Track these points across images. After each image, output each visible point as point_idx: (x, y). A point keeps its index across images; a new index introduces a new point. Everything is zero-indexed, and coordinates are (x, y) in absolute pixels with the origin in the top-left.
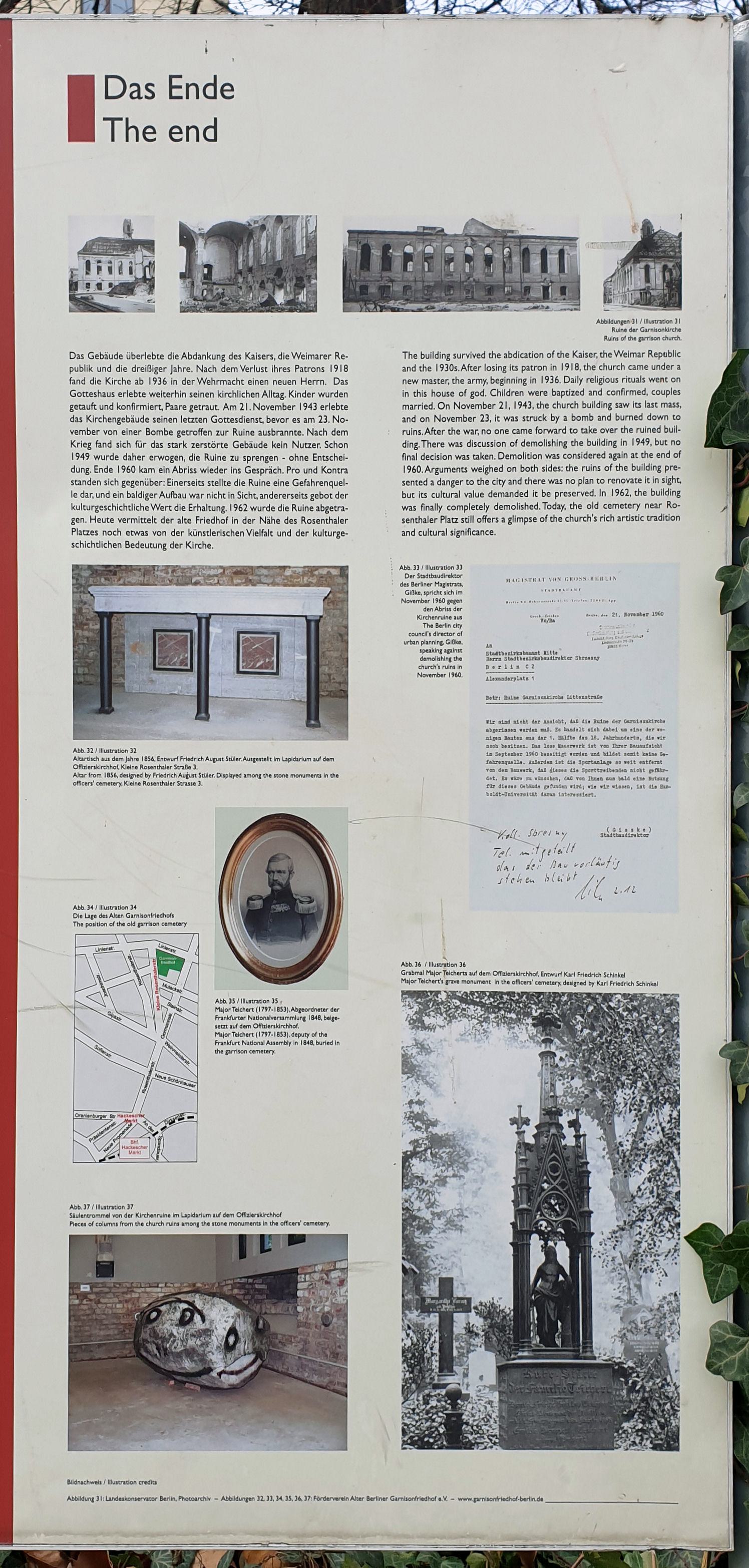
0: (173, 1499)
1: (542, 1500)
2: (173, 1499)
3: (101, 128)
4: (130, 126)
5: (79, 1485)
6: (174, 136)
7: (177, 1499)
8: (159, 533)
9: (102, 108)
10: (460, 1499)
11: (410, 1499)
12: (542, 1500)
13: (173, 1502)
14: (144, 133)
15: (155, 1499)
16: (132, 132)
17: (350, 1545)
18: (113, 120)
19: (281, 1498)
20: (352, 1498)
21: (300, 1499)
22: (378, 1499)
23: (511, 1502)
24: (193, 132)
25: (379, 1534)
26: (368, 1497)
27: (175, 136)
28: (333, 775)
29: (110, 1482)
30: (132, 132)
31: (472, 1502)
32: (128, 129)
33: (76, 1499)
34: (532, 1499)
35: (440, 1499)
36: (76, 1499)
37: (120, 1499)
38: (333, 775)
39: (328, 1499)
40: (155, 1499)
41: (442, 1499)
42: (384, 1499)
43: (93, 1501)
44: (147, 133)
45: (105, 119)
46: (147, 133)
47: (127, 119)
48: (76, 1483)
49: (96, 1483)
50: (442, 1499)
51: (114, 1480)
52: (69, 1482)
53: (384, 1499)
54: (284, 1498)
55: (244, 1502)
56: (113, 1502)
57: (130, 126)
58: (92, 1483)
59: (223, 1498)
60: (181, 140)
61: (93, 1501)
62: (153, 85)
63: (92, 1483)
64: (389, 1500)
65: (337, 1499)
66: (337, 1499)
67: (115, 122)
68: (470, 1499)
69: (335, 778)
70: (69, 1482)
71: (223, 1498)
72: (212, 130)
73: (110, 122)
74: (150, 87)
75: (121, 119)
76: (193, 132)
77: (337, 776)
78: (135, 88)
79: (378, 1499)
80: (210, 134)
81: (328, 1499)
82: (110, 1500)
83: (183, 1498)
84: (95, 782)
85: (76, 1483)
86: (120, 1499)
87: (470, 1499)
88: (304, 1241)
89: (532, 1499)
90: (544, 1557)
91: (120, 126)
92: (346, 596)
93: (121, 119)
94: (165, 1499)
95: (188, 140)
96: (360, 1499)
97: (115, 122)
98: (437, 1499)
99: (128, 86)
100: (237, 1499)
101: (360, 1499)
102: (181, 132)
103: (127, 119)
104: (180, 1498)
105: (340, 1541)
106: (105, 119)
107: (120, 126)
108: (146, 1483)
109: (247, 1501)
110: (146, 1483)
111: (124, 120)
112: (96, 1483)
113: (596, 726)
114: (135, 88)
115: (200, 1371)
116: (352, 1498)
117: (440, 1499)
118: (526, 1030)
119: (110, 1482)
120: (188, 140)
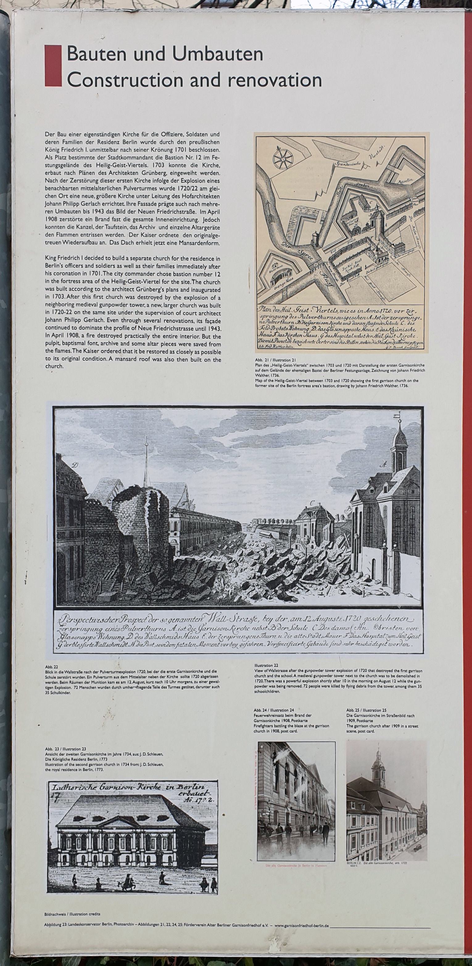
1: (328, 926)
6: (240, 83)
7: (113, 924)
9: (67, 66)
10: (276, 926)
12: (328, 926)
15: (99, 924)
17: (107, 953)
19: (175, 925)
20: (208, 925)
22: (224, 925)
23: (308, 928)
24: (251, 81)
25: (166, 948)
27: (240, 83)
28: (414, 381)
29: (71, 914)
34: (322, 926)
35: (263, 926)
37: (77, 925)
38: (414, 381)
40: (99, 924)
41: (265, 925)
42: (228, 926)
43: (60, 926)
48: (50, 915)
49: (62, 915)
50: (265, 925)
51: (74, 913)
52: (46, 914)
53: (228, 926)
54: (177, 925)
56: (73, 926)
58: (60, 915)
59: (139, 924)
60: (244, 85)
61: (60, 926)
63: (60, 915)
64: (231, 926)
65: (199, 925)
68: (282, 926)
69: (416, 383)
70: (46, 914)
71: (139, 924)
76: (251, 81)
77: (417, 381)
78: (83, 54)
79: (224, 925)
81: (193, 925)
82: (71, 925)
83: (117, 924)
85: (50, 915)
86: (77, 925)
87: (282, 926)
88: (75, 818)
89: (322, 926)
90: (59, 959)
95: (248, 86)
96: (213, 925)
98: (262, 925)
99: (215, 53)
100: (148, 925)
101: (213, 925)
102: (244, 81)
104: (115, 923)
105: (139, 951)
108: (93, 914)
110: (93, 914)
112: (62, 915)
114: (219, 54)
116: (208, 925)
117: (263, 926)
119: (71, 914)
120: (248, 86)
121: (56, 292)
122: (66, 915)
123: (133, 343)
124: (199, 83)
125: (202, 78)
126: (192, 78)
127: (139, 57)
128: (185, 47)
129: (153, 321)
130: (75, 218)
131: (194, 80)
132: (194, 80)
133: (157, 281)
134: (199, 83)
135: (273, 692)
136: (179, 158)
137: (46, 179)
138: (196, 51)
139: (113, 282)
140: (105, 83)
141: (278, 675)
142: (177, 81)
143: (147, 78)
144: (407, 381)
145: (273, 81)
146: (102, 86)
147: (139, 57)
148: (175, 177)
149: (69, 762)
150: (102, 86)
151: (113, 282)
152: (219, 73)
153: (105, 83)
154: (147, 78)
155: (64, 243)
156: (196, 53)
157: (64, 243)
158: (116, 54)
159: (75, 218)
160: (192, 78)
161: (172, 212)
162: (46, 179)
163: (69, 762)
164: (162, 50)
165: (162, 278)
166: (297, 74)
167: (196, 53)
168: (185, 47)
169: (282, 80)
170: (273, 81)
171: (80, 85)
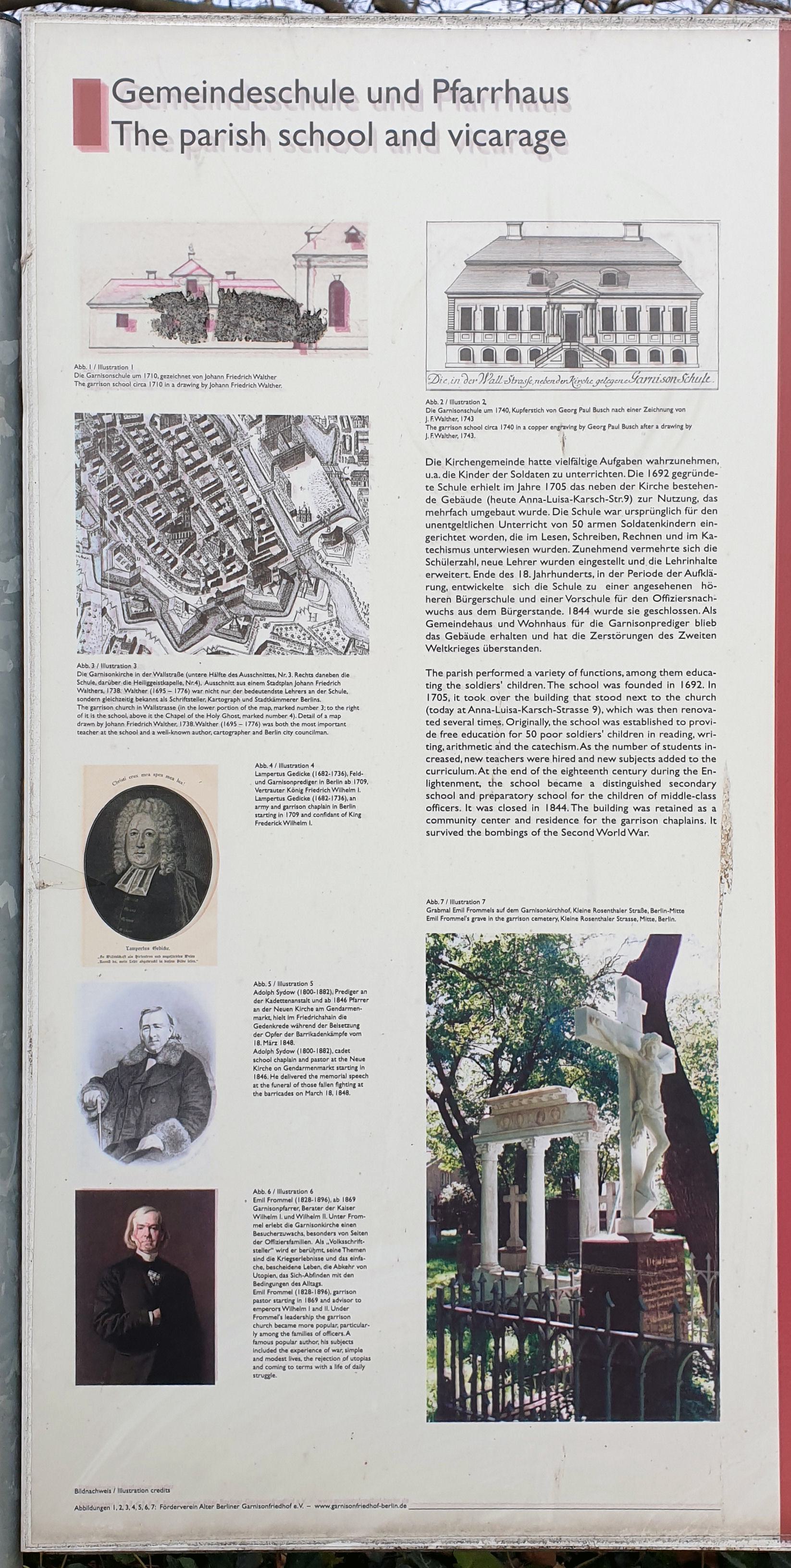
4: (256, 129)
5: (87, 1494)
9: (114, 110)
11: (263, 1507)
12: (405, 1506)
14: (155, 136)
16: (142, 135)
18: (122, 124)
23: (371, 1509)
29: (120, 1491)
30: (142, 135)
31: (330, 1509)
32: (137, 132)
35: (295, 1507)
44: (158, 138)
46: (158, 138)
47: (137, 123)
49: (105, 1491)
55: (99, 1511)
57: (256, 129)
62: (566, 89)
66: (185, 1507)
67: (125, 125)
68: (328, 1507)
73: (119, 125)
74: (563, 92)
75: (130, 123)
78: (529, 92)
80: (428, 138)
84: (606, 733)
87: (328, 1507)
93: (130, 123)
97: (125, 125)
103: (137, 123)
108: (158, 1491)
109: (101, 1511)
110: (158, 1491)
112: (105, 1491)
114: (529, 92)
115: (473, 1367)
119: (120, 1491)
121: (463, 431)
124: (212, 141)
125: (405, 133)
126: (388, 132)
127: (375, 97)
131: (392, 135)
132: (392, 135)
134: (212, 141)
135: (293, 823)
138: (170, 88)
140: (236, 138)
141: (566, 776)
142: (367, 138)
143: (484, 132)
144: (469, 513)
145: (456, 137)
146: (231, 144)
147: (375, 97)
150: (231, 144)
152: (433, 124)
153: (236, 138)
154: (484, 132)
156: (169, 91)
158: (155, 91)
160: (388, 132)
164: (239, 86)
166: (468, 125)
167: (169, 91)
169: (525, 135)
170: (456, 137)
171: (485, 144)
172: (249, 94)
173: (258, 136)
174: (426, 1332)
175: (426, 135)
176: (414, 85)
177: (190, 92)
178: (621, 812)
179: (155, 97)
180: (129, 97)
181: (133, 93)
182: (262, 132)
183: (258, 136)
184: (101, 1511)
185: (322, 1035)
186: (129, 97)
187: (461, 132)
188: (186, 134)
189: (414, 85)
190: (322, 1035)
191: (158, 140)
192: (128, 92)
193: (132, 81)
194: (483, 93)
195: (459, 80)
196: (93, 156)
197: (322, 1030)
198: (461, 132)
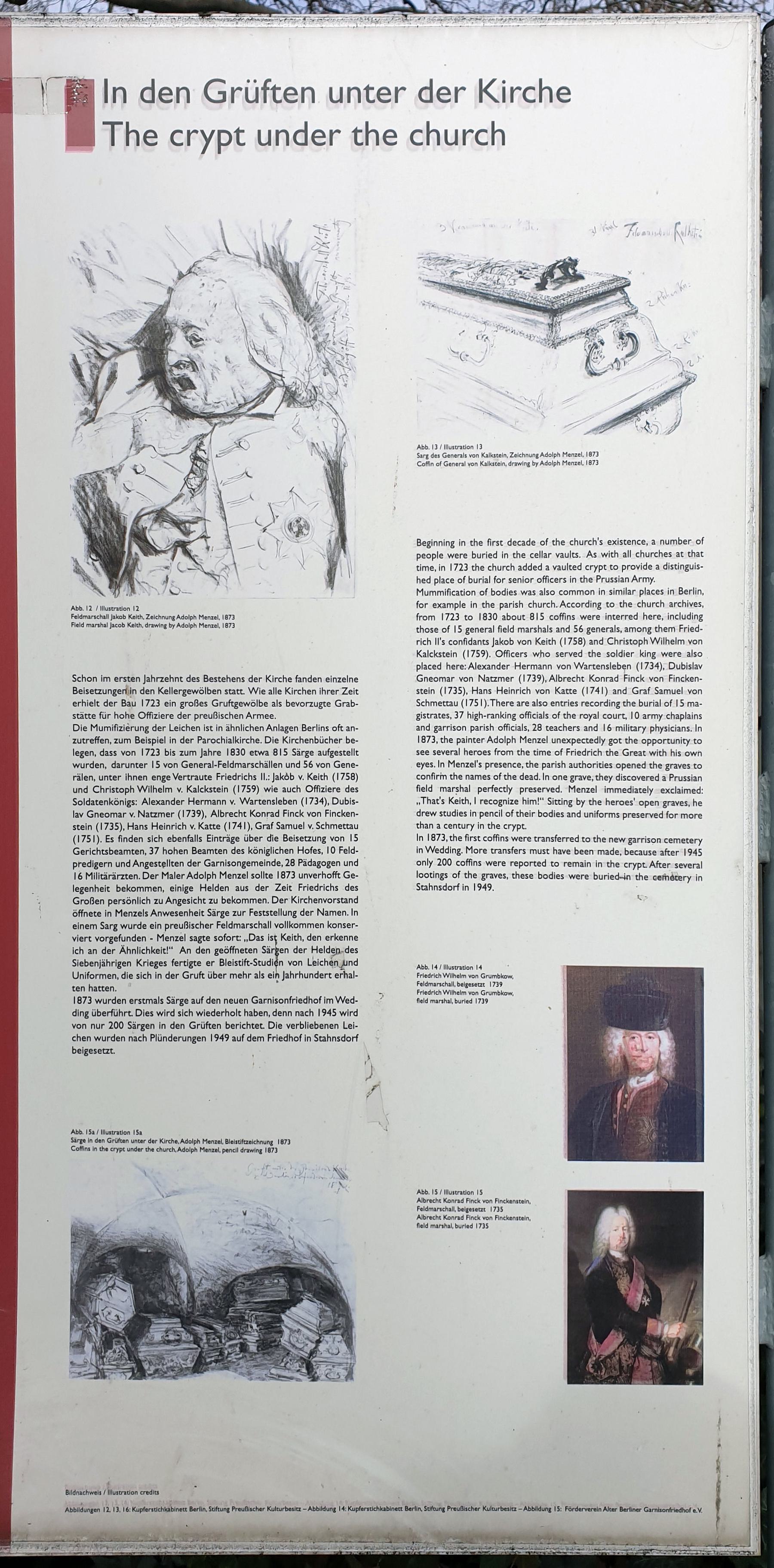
0: (417, 1509)
2: (417, 1509)
3: (101, 134)
4: (431, 129)
8: (302, 704)
9: (102, 112)
13: (204, 1512)
14: (145, 137)
16: (133, 136)
18: (113, 124)
21: (127, 1510)
22: (631, 1510)
26: (621, 1508)
30: (133, 136)
32: (128, 133)
33: (533, 1509)
35: (694, 1511)
36: (317, 1509)
39: (580, 1510)
41: (697, 1510)
45: (104, 123)
47: (127, 123)
49: (95, 1493)
50: (697, 1510)
55: (89, 1513)
63: (92, 1493)
64: (642, 1511)
65: (589, 1510)
66: (589, 1510)
72: (223, 141)
73: (109, 126)
75: (121, 123)
81: (580, 1510)
91: (120, 131)
92: (698, 1159)
93: (121, 123)
94: (410, 1509)
98: (692, 1511)
103: (127, 123)
106: (104, 123)
107: (120, 131)
109: (92, 1512)
111: (124, 124)
112: (95, 1493)
113: (612, 549)
117: (694, 1511)
118: (162, 303)
122: (102, 1493)
123: (215, 937)
127: (336, 97)
128: (106, 81)
129: (447, 753)
130: (119, 800)
133: (593, 789)
136: (281, 1001)
137: (139, 812)
139: (203, 890)
145: (208, 136)
148: (326, 759)
149: (516, 808)
151: (203, 890)
155: (338, 1002)
157: (338, 1002)
158: (299, 92)
159: (119, 800)
161: (322, 888)
162: (139, 812)
163: (516, 808)
165: (493, 574)
168: (106, 81)
170: (208, 136)
172: (160, 94)
173: (498, 136)
174: (69, 1353)
175: (299, 135)
176: (150, 85)
177: (562, 91)
178: (566, 806)
179: (174, 97)
180: (221, 97)
181: (224, 93)
182: (503, 132)
183: (498, 136)
184: (92, 1512)
185: (175, 1039)
186: (221, 97)
187: (213, 132)
188: (222, 135)
189: (150, 85)
190: (175, 1039)
191: (388, 140)
192: (220, 93)
193: (224, 82)
194: (237, 93)
195: (269, 80)
196: (80, 156)
197: (176, 1033)
198: (213, 132)
